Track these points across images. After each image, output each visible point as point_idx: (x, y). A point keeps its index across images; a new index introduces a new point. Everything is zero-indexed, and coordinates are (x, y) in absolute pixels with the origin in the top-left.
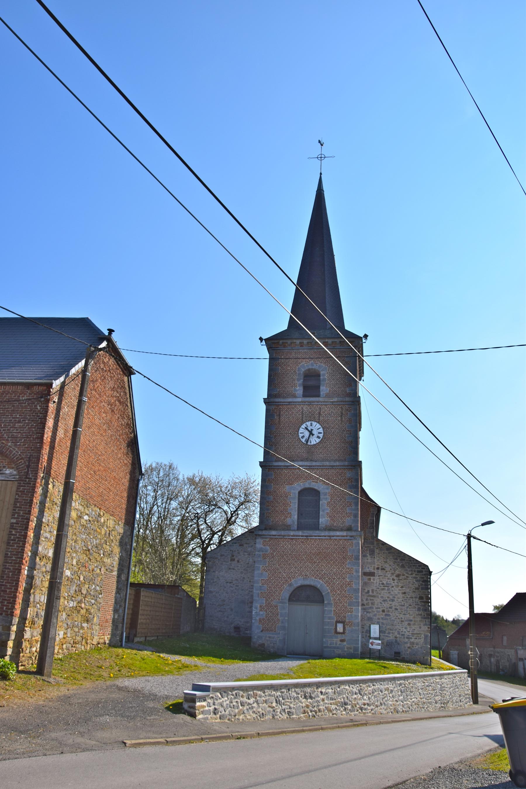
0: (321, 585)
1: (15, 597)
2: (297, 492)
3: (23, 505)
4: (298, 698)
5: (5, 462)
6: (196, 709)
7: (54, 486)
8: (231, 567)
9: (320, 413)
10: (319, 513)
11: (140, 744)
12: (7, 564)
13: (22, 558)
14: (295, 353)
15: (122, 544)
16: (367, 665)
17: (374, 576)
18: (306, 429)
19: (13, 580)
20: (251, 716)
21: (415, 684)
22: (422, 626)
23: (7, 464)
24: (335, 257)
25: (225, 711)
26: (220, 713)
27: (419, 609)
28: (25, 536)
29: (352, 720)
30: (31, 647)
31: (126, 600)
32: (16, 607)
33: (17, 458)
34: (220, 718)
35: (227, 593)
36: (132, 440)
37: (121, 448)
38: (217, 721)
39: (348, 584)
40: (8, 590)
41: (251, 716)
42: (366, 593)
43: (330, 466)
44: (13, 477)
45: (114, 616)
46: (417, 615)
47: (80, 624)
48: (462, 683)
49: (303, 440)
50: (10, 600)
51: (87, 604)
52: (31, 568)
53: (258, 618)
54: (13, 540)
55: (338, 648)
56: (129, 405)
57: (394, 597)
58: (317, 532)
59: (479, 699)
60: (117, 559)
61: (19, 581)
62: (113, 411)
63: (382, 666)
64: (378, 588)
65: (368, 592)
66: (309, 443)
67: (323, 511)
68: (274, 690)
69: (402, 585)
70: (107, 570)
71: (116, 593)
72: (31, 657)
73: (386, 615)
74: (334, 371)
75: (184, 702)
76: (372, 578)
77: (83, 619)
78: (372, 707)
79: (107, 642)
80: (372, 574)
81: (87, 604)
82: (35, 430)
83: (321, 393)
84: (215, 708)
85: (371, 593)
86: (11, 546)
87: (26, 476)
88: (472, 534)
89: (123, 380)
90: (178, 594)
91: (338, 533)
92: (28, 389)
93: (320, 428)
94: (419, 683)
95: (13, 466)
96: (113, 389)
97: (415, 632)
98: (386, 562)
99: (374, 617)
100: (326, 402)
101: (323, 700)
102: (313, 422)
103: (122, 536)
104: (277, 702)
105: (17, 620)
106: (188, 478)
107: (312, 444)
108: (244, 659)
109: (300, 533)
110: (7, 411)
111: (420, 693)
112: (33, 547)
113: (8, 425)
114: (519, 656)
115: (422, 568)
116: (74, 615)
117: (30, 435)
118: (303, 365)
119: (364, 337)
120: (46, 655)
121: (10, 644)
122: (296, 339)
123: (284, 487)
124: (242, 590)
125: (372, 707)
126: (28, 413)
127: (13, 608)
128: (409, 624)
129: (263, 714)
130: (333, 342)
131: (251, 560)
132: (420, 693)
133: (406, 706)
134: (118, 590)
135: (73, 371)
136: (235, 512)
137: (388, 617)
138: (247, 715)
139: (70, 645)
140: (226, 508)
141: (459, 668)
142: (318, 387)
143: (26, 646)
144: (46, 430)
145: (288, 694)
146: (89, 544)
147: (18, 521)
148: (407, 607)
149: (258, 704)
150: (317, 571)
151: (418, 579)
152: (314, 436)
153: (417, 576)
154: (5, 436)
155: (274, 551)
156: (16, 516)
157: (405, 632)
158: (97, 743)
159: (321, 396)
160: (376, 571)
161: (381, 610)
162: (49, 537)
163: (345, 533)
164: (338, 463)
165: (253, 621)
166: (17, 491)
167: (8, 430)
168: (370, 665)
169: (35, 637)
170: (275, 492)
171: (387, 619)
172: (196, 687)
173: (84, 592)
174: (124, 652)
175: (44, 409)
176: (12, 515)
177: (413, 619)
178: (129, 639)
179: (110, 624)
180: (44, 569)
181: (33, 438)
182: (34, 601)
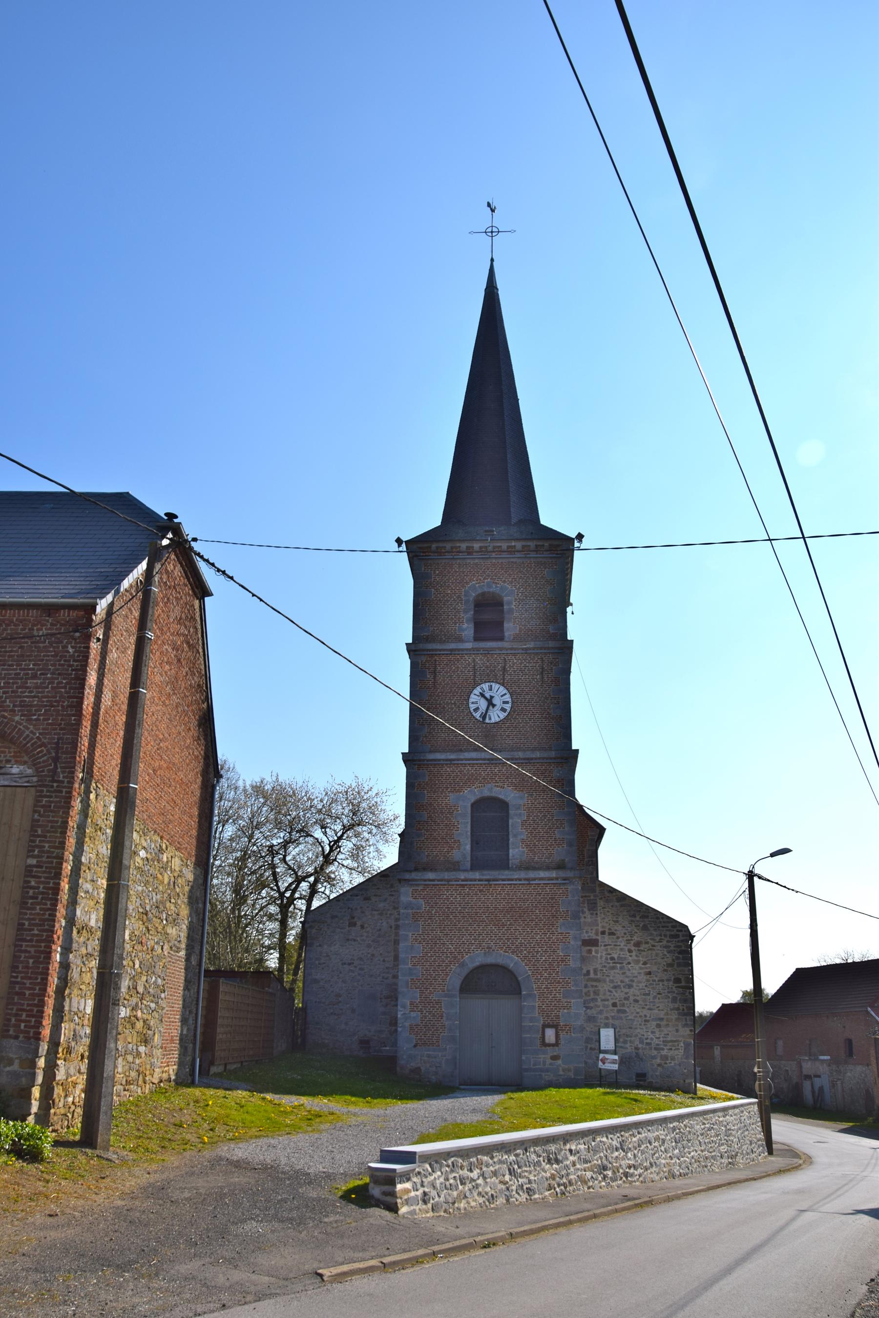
0: (516, 963)
1: (42, 1004)
2: (469, 805)
3: (49, 832)
4: (539, 1163)
5: (10, 752)
6: (396, 1197)
7: (97, 795)
8: (350, 937)
9: (504, 669)
10: (508, 840)
11: (344, 1274)
12: (24, 944)
13: (53, 932)
14: (459, 564)
15: (192, 901)
16: (606, 1097)
17: (597, 946)
18: (482, 695)
19: (37, 973)
20: (475, 1201)
21: (692, 1127)
22: (680, 1027)
23: (13, 757)
24: (520, 401)
25: (439, 1196)
26: (432, 1201)
27: (674, 1000)
28: (57, 889)
29: (626, 1198)
30: (66, 1096)
31: (198, 1000)
32: (44, 1023)
33: (32, 745)
34: (433, 1210)
35: (344, 982)
36: (204, 714)
37: (190, 729)
38: (428, 1215)
39: (563, 961)
40: (27, 992)
41: (476, 1201)
42: (584, 975)
43: (524, 759)
44: (27, 779)
45: (182, 1031)
46: (671, 1010)
47: (135, 1047)
48: (752, 1121)
49: (477, 715)
50: (32, 1011)
51: (145, 1011)
52: (66, 949)
53: (407, 1024)
54: (32, 898)
55: (547, 1070)
56: (201, 650)
57: (632, 981)
58: (506, 872)
59: (774, 1146)
60: (184, 927)
61: (48, 974)
62: (179, 661)
63: (632, 1099)
64: (605, 966)
65: (588, 972)
66: (487, 721)
67: (515, 836)
68: (506, 1153)
69: (644, 960)
70: (171, 948)
71: (184, 990)
72: (65, 1115)
73: (619, 1011)
74: (526, 596)
75: (372, 1185)
76: (594, 949)
77: (139, 1039)
78: (640, 1171)
79: (173, 1077)
80: (594, 943)
81: (145, 1011)
82: (66, 692)
83: (506, 634)
84: (424, 1192)
85: (592, 975)
86: (29, 909)
87: (53, 777)
88: (756, 871)
89: (193, 606)
90: (269, 987)
91: (542, 874)
92: (49, 616)
93: (505, 694)
94: (697, 1124)
95: (26, 758)
96: (179, 621)
97: (669, 1039)
98: (617, 922)
99: (600, 1016)
100: (515, 649)
101: (574, 1164)
102: (493, 684)
103: (192, 887)
104: (510, 1174)
105: (46, 1047)
106: (252, 787)
107: (493, 721)
108: (402, 1098)
109: (477, 875)
110: (9, 656)
111: (700, 1143)
112: (69, 910)
113: (13, 683)
114: (805, 1072)
115: (678, 931)
116: (127, 1031)
117: (55, 702)
118: (474, 585)
119: (577, 537)
120: (99, 1110)
121: (36, 1092)
122: (460, 541)
123: (446, 797)
124: (371, 976)
125: (640, 1171)
126: (50, 660)
127: (39, 1024)
128: (658, 1026)
129: (492, 1195)
130: (523, 547)
131: (384, 924)
132: (700, 1143)
133: (683, 1166)
134: (188, 982)
135: (126, 584)
136: (335, 845)
137: (622, 1015)
138: (470, 1200)
139: (122, 1087)
140: (318, 833)
141: (739, 1096)
142: (500, 624)
143: (58, 1094)
144: (87, 691)
145: (525, 1157)
146: (147, 901)
147: (41, 861)
148: (655, 997)
149: (485, 1178)
150: (508, 939)
151: (672, 948)
152: (496, 708)
153: (669, 944)
154: (8, 703)
155: (432, 907)
156: (36, 852)
157: (652, 1039)
158: (273, 1280)
159: (506, 639)
160: (599, 937)
161: (610, 1003)
162: (91, 891)
163: (554, 874)
164: (538, 754)
165: (399, 1029)
166: (35, 806)
167: (12, 692)
168: (612, 1098)
169: (71, 1076)
170: (431, 804)
171: (621, 1018)
172: (387, 1157)
173: (141, 989)
174: (204, 1094)
175: (81, 652)
176: (29, 851)
177: (665, 1017)
178: (204, 1072)
179: (176, 1045)
180: (84, 951)
181: (63, 706)
182: (70, 1011)
